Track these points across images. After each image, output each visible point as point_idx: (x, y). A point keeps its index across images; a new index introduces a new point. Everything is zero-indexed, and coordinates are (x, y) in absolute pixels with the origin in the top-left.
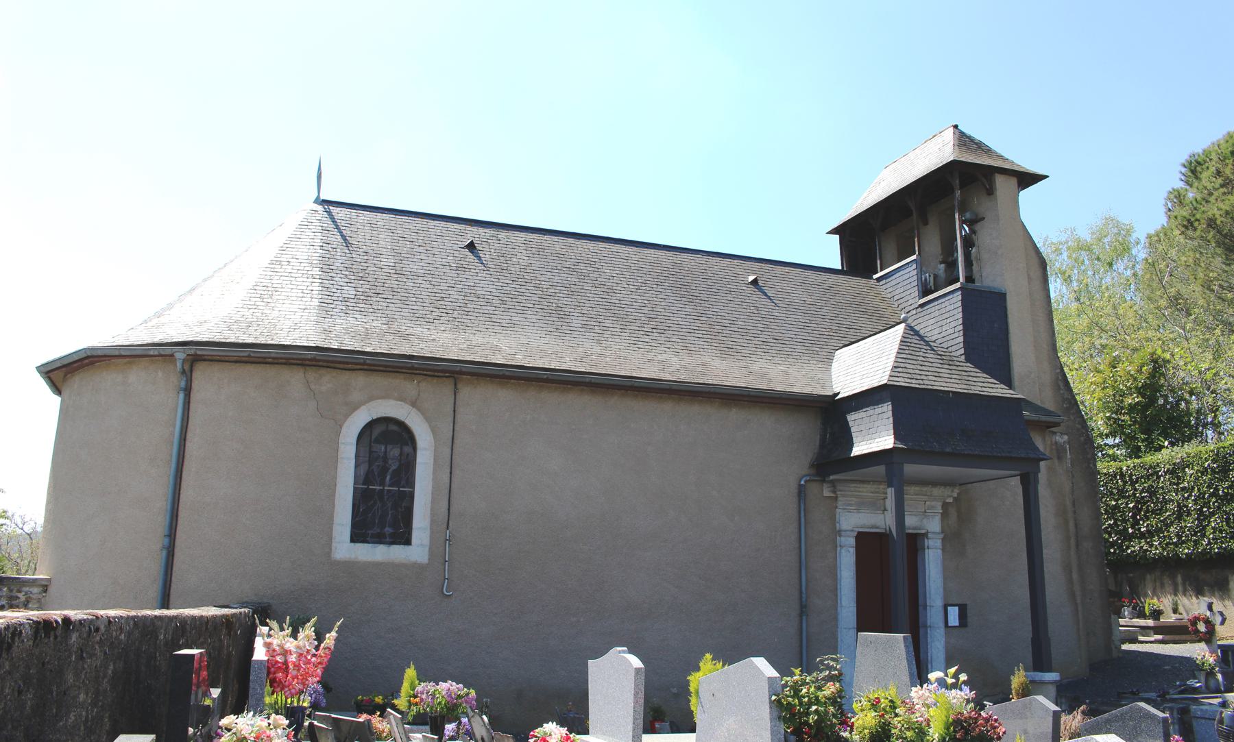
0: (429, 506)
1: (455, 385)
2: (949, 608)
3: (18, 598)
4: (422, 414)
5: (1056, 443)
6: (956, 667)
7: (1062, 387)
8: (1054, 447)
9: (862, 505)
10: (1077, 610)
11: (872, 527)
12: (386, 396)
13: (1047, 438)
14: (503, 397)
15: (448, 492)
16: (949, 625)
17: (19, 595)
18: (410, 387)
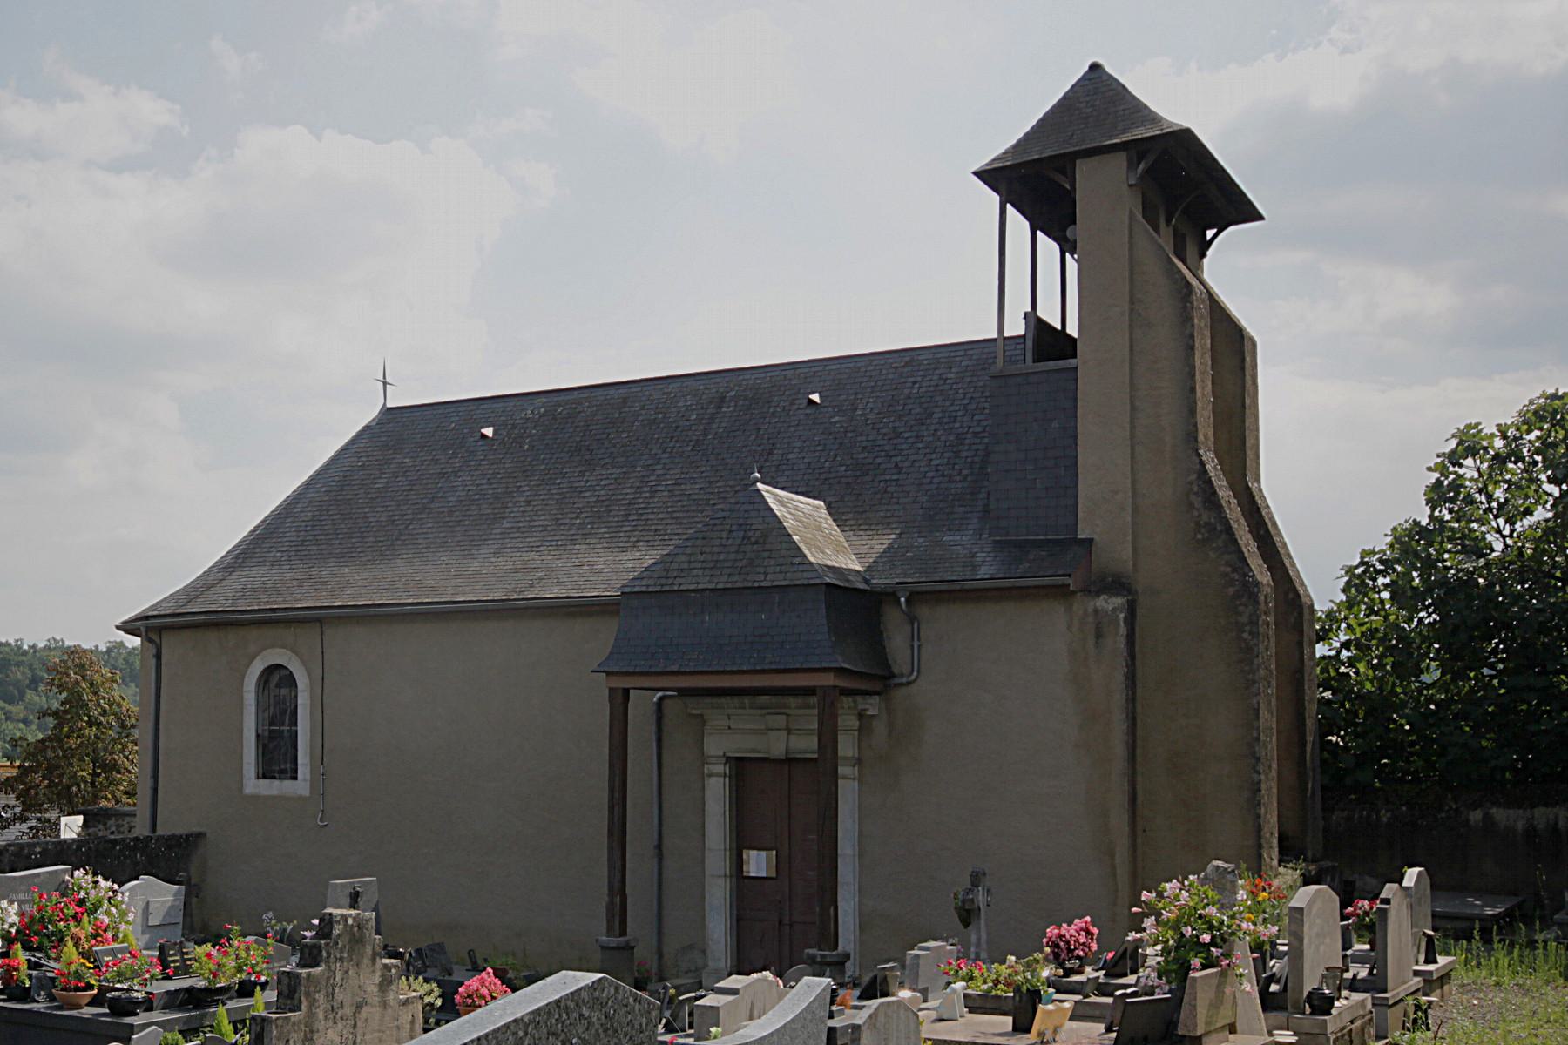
3: (123, 825)
5: (1096, 611)
13: (1075, 607)
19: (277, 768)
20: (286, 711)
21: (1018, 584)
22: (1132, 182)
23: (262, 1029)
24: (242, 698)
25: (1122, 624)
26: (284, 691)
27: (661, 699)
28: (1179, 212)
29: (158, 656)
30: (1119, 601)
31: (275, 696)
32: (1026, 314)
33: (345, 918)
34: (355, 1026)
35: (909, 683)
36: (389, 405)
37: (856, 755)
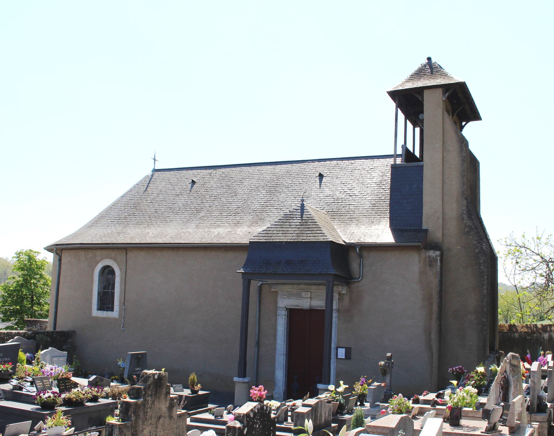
0: (119, 297)
1: (126, 252)
2: (339, 349)
3: (42, 326)
4: (117, 263)
5: (429, 257)
6: (450, 381)
7: (465, 218)
8: (427, 259)
9: (290, 295)
10: (432, 356)
11: (296, 306)
12: (106, 258)
13: (422, 255)
14: (142, 255)
15: (124, 292)
16: (338, 357)
17: (43, 326)
18: (113, 253)
19: (106, 306)
20: (110, 284)
21: (401, 245)
22: (444, 99)
23: (112, 430)
24: (93, 278)
25: (439, 261)
26: (110, 276)
27: (261, 285)
28: (455, 115)
29: (60, 260)
30: (438, 253)
31: (106, 278)
32: (402, 145)
33: (154, 375)
34: (157, 427)
35: (359, 281)
36: (156, 168)
37: (337, 308)
